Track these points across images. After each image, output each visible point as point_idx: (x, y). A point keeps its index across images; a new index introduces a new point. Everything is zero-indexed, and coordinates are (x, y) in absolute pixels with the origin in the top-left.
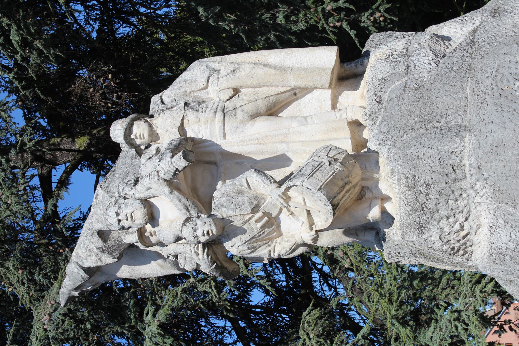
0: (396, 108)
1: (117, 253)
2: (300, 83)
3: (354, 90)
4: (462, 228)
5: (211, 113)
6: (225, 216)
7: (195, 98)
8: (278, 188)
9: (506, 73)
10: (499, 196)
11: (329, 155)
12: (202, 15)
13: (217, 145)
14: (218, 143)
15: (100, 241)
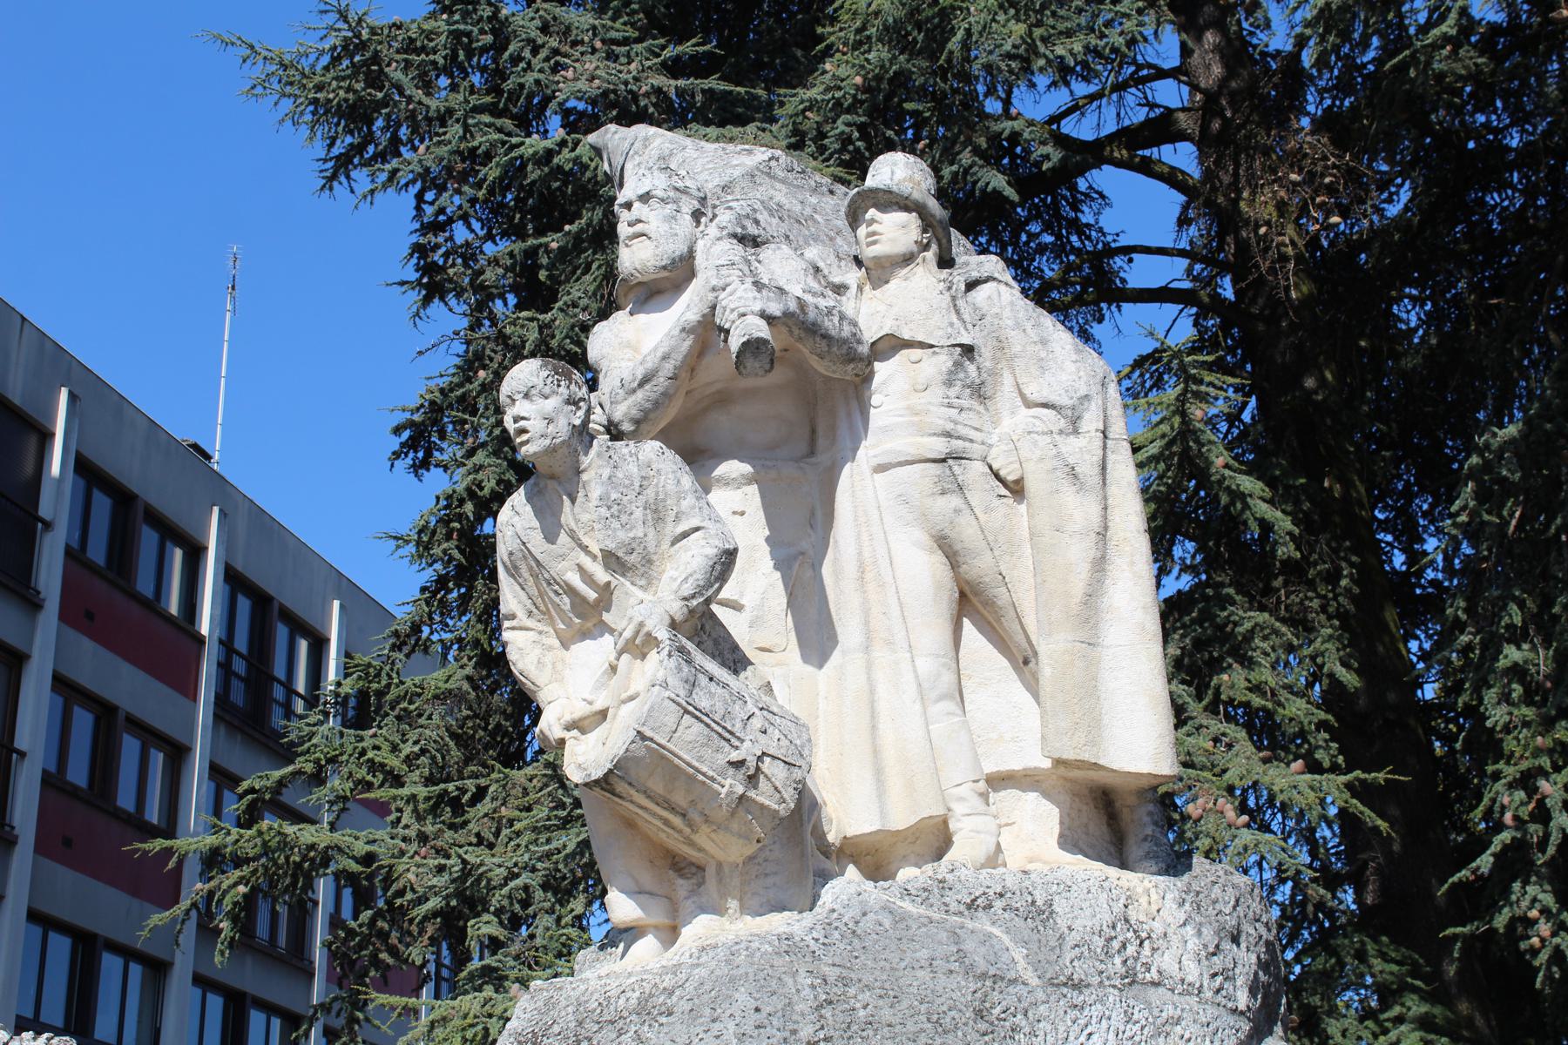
0: (924, 954)
2: (1047, 669)
3: (1061, 836)
5: (941, 422)
6: (584, 477)
7: (994, 373)
8: (667, 621)
11: (767, 760)
12: (1495, 435)
13: (855, 450)
14: (861, 453)
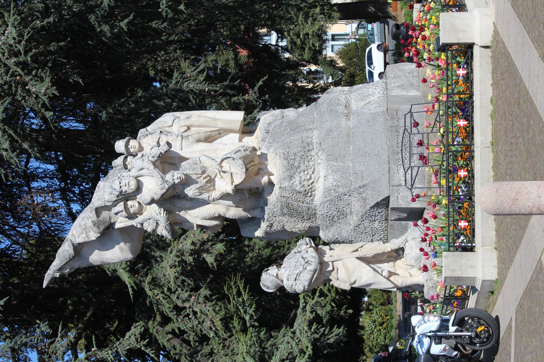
1: (102, 228)
4: (311, 178)
9: (334, 103)
10: (331, 157)
15: (95, 216)
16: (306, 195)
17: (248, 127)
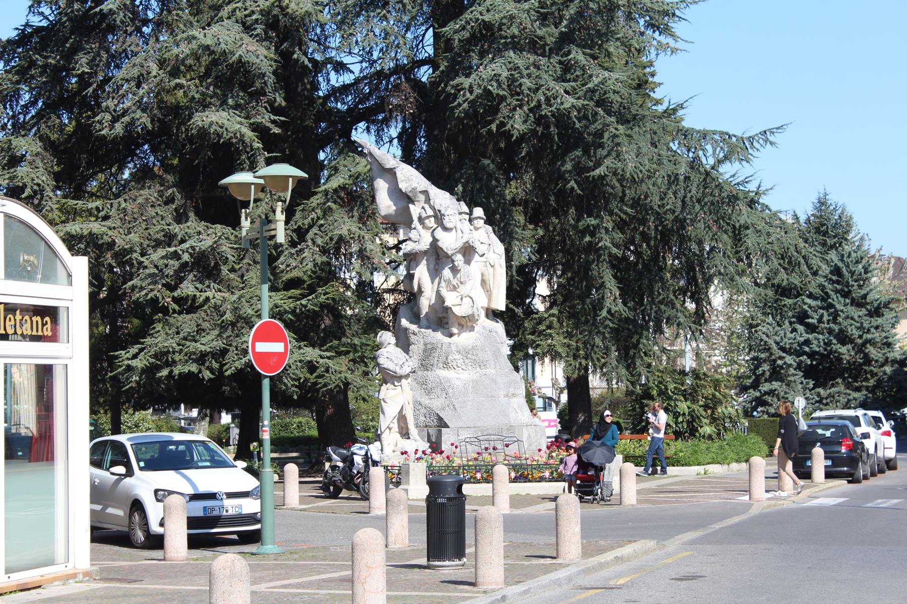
1: (410, 194)
10: (475, 383)
16: (445, 363)
17: (494, 314)
